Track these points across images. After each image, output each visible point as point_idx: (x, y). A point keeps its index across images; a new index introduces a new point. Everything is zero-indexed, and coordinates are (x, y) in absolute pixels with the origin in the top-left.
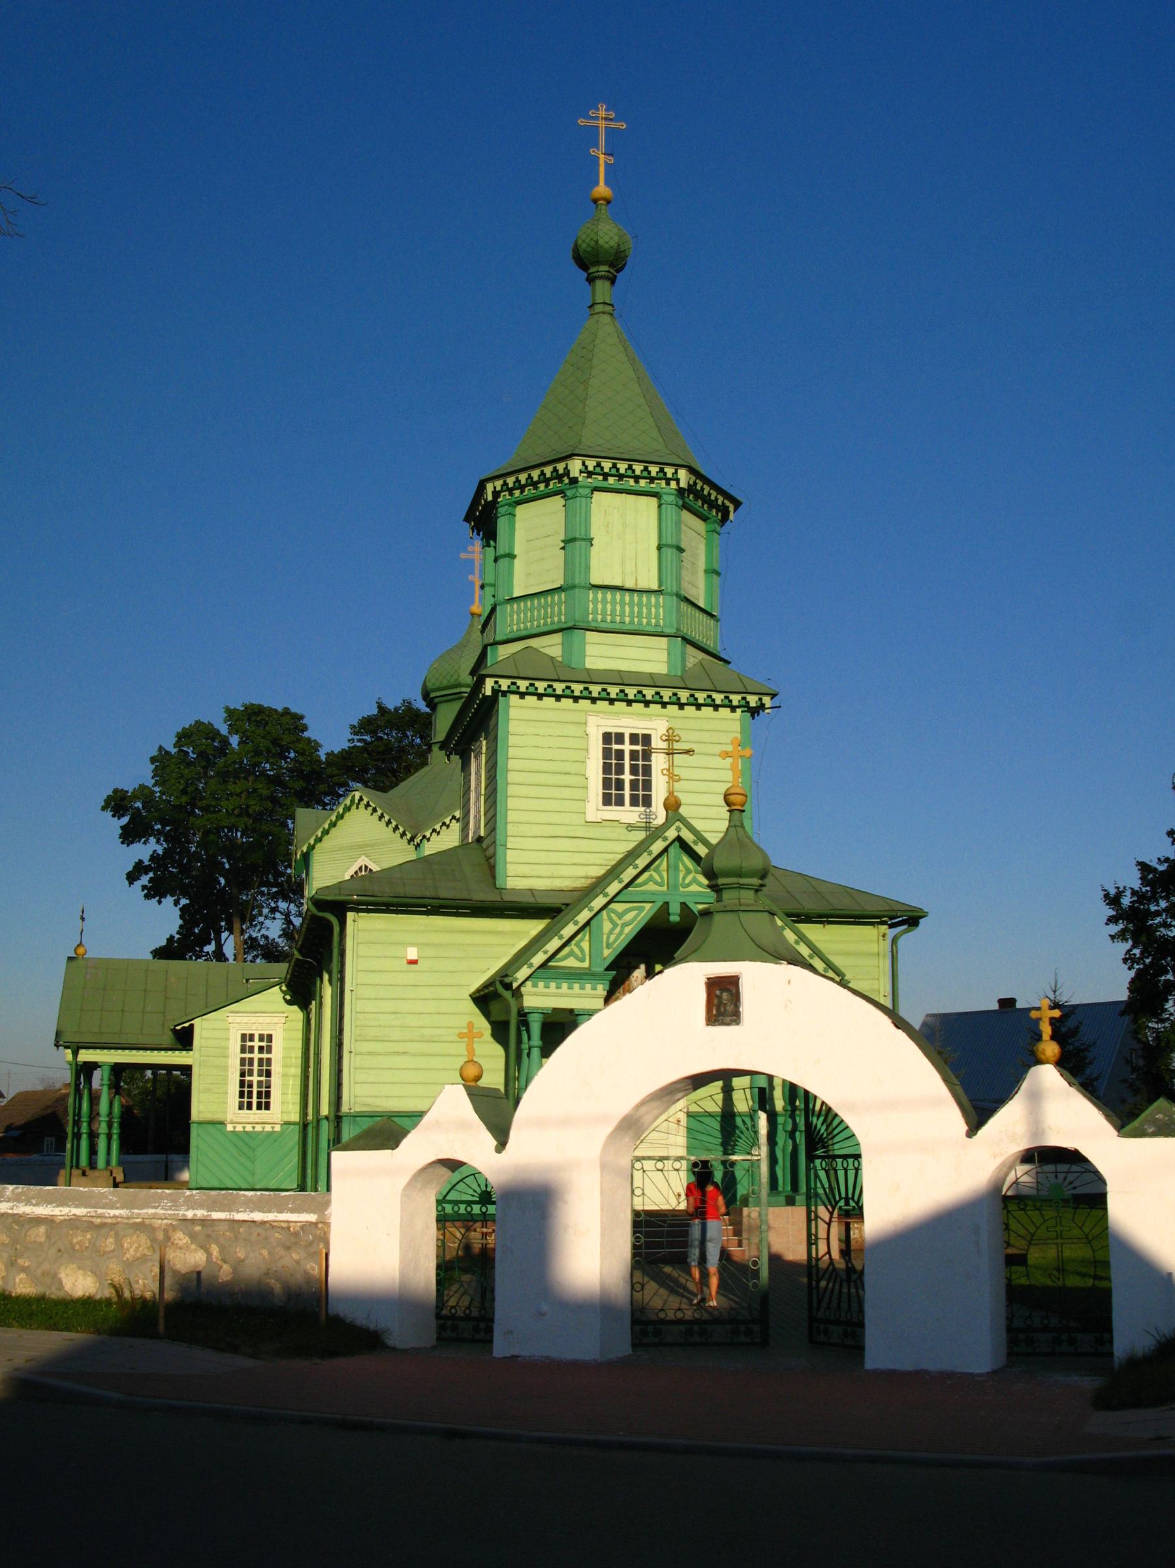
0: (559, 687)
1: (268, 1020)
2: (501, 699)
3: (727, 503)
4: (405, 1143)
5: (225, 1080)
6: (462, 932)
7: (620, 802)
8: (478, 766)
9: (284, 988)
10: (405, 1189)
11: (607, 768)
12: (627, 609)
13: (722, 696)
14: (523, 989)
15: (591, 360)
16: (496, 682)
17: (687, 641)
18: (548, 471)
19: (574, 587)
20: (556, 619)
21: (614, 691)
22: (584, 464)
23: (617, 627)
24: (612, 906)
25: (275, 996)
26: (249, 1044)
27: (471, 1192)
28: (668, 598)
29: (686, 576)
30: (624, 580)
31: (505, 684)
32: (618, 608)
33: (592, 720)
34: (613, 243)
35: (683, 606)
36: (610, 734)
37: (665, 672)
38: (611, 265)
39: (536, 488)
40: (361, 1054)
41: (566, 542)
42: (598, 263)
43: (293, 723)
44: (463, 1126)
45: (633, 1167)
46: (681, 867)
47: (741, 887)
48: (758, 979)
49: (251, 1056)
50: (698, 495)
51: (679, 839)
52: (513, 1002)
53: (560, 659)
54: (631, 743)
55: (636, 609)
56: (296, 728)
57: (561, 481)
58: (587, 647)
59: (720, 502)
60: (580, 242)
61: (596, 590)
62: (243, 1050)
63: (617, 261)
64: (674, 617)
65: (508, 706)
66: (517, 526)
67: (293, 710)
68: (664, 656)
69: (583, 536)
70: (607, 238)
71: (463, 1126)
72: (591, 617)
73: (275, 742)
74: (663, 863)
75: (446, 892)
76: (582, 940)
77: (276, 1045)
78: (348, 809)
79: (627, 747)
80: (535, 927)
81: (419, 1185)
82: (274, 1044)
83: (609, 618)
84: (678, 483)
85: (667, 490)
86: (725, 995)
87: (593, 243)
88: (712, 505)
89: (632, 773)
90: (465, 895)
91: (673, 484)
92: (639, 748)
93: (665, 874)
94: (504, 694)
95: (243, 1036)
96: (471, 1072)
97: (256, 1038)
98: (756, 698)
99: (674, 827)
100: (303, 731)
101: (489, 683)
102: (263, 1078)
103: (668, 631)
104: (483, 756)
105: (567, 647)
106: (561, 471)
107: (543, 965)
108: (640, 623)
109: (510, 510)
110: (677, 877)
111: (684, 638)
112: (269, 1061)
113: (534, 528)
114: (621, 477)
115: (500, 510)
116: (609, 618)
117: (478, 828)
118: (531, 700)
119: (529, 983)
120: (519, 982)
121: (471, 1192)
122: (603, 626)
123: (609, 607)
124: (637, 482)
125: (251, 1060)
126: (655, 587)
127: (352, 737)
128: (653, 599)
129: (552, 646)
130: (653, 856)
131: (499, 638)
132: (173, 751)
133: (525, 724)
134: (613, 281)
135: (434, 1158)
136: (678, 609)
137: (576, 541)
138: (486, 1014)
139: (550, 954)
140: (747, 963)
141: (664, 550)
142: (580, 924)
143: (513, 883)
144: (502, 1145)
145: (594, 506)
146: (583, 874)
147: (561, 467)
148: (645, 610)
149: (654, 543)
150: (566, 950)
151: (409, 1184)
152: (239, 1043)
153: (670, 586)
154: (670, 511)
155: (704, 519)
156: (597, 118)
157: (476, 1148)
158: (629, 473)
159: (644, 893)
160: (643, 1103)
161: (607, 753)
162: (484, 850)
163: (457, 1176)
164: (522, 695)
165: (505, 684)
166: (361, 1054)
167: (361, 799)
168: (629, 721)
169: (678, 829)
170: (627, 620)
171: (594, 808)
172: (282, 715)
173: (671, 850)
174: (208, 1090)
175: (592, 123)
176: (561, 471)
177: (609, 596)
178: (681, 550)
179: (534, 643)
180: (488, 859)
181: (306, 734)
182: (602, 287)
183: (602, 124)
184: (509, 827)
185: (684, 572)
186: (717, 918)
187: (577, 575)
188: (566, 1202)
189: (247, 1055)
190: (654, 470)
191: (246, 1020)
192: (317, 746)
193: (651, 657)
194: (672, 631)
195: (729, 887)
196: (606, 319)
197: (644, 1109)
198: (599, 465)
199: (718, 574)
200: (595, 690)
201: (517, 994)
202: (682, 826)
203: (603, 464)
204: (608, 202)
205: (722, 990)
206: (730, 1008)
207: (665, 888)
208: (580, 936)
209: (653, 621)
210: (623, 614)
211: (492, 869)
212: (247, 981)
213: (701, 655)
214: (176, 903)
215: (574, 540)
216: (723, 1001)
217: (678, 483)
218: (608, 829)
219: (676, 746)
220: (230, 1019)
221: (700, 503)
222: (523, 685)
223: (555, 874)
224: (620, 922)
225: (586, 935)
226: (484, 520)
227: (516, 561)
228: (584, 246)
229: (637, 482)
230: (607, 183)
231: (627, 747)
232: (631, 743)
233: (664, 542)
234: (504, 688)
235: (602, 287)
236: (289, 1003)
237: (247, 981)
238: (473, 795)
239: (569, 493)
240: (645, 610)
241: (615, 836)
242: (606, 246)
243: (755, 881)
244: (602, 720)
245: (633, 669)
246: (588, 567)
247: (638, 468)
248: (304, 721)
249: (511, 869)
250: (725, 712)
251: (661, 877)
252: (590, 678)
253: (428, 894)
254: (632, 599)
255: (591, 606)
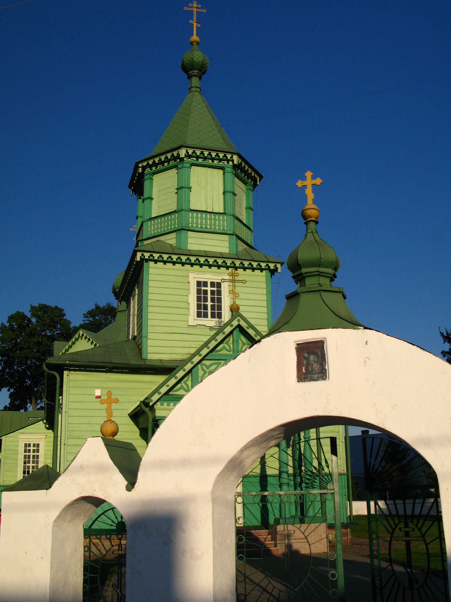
0: (175, 257)
1: (37, 437)
2: (145, 264)
3: (256, 176)
4: (56, 484)
5: (16, 465)
6: (125, 381)
7: (206, 316)
8: (134, 303)
9: (45, 421)
10: (55, 521)
11: (199, 299)
12: (208, 221)
13: (256, 263)
14: (155, 406)
15: (190, 110)
16: (143, 255)
17: (238, 237)
18: (169, 155)
19: (182, 210)
20: (173, 226)
21: (202, 260)
22: (187, 152)
23: (204, 230)
24: (204, 362)
25: (41, 426)
26: (28, 448)
27: (110, 522)
28: (228, 216)
29: (237, 209)
30: (207, 208)
31: (147, 255)
32: (204, 221)
33: (191, 275)
34: (200, 60)
35: (236, 222)
36: (201, 282)
37: (228, 252)
38: (200, 70)
39: (163, 165)
40: (70, 445)
41: (177, 189)
42: (193, 69)
43: (60, 312)
44: (101, 468)
45: (236, 501)
46: (240, 342)
47: (320, 274)
48: (339, 342)
49: (29, 454)
50: (243, 170)
51: (239, 326)
52: (150, 414)
53: (175, 245)
54: (211, 287)
55: (213, 222)
56: (61, 315)
57: (175, 161)
58: (189, 239)
59: (253, 175)
60: (185, 59)
61: (193, 212)
62: (25, 451)
63: (202, 70)
64: (232, 226)
65: (149, 267)
66: (154, 184)
67: (59, 307)
68: (227, 244)
69: (186, 186)
70: (197, 57)
71: (101, 468)
72: (190, 225)
73: (52, 320)
74: (231, 339)
75: (116, 360)
76: (187, 380)
77: (41, 449)
78: (77, 339)
79: (209, 289)
80: (161, 379)
81: (68, 518)
82: (40, 448)
83: (199, 226)
84: (233, 163)
85: (228, 165)
86: (312, 358)
87: (191, 60)
88: (249, 176)
89: (211, 302)
90: (126, 362)
91: (231, 163)
92: (215, 289)
93: (231, 346)
94: (147, 260)
95: (26, 445)
96: (110, 428)
97: (32, 445)
98: (273, 265)
99: (236, 319)
100: (63, 316)
101: (139, 255)
102: (35, 465)
103: (228, 232)
104: (136, 296)
105: (178, 239)
106: (175, 155)
107: (167, 393)
108: (215, 228)
109: (150, 177)
110: (238, 346)
111: (237, 236)
112: (38, 456)
113: (162, 189)
114: (205, 158)
115: (145, 177)
116: (199, 226)
117: (133, 332)
118: (160, 264)
119: (159, 403)
120: (154, 402)
121: (110, 522)
122: (197, 229)
123: (199, 220)
124: (213, 161)
125: (29, 456)
126: (222, 211)
127: (84, 319)
128: (221, 217)
129: (171, 240)
130: (226, 335)
131: (144, 238)
132: (7, 325)
133: (157, 275)
134: (200, 79)
135: (77, 496)
136: (234, 222)
137: (183, 189)
138: (137, 424)
139: (170, 387)
140: (330, 330)
141: (226, 194)
142: (187, 371)
143: (151, 357)
144: (131, 485)
145: (192, 173)
146: (187, 352)
147: (175, 153)
148: (217, 222)
149: (222, 192)
150: (179, 386)
151: (59, 517)
152: (23, 448)
153: (229, 211)
154: (230, 176)
155: (245, 183)
156: (192, 7)
157: (111, 487)
158: (209, 157)
159: (220, 355)
160: (246, 447)
161: (199, 291)
162: (138, 343)
163: (100, 510)
164: (156, 262)
165: (147, 255)
166: (70, 445)
167: (83, 335)
168: (210, 275)
169: (239, 321)
170: (209, 227)
171: (193, 319)
172: (54, 309)
173: (235, 332)
174: (8, 471)
175: (190, 9)
176: (175, 155)
177: (208, 216)
178: (235, 195)
179: (162, 238)
180: (138, 346)
181: (65, 318)
182: (195, 81)
183: (195, 10)
184: (149, 328)
185: (236, 207)
186: (303, 297)
187: (183, 204)
188: (184, 531)
189: (27, 454)
190: (221, 155)
191: (27, 437)
192: (70, 323)
193: (221, 245)
194: (231, 232)
195: (311, 275)
196: (197, 94)
197: (246, 453)
198: (194, 152)
199: (252, 210)
200: (193, 259)
201: (152, 409)
202: (240, 319)
203: (196, 152)
204: (198, 44)
205: (310, 353)
206: (316, 367)
207: (232, 353)
208: (186, 378)
209: (222, 228)
210: (206, 224)
211: (140, 350)
212: (28, 418)
213: (245, 246)
214: (9, 390)
215: (182, 188)
216: (312, 363)
217: (233, 163)
218: (199, 330)
219: (236, 278)
220: (19, 437)
221: (243, 175)
222: (156, 256)
223: (173, 352)
224: (208, 371)
225: (190, 376)
226: (138, 186)
227: (153, 201)
228: (187, 61)
229: (213, 161)
230: (197, 35)
231: (209, 289)
232: (211, 287)
233: (226, 190)
234: (147, 257)
235: (195, 81)
236: (48, 429)
237: (28, 418)
238: (131, 318)
239: (179, 166)
240: (217, 222)
241: (203, 333)
242: (197, 61)
243: (330, 271)
244: (195, 275)
245: (212, 250)
246: (189, 201)
247: (214, 154)
248: (64, 312)
249: (150, 349)
250: (257, 272)
251: (230, 347)
252: (190, 254)
253: (106, 361)
254: (211, 217)
255: (190, 220)
